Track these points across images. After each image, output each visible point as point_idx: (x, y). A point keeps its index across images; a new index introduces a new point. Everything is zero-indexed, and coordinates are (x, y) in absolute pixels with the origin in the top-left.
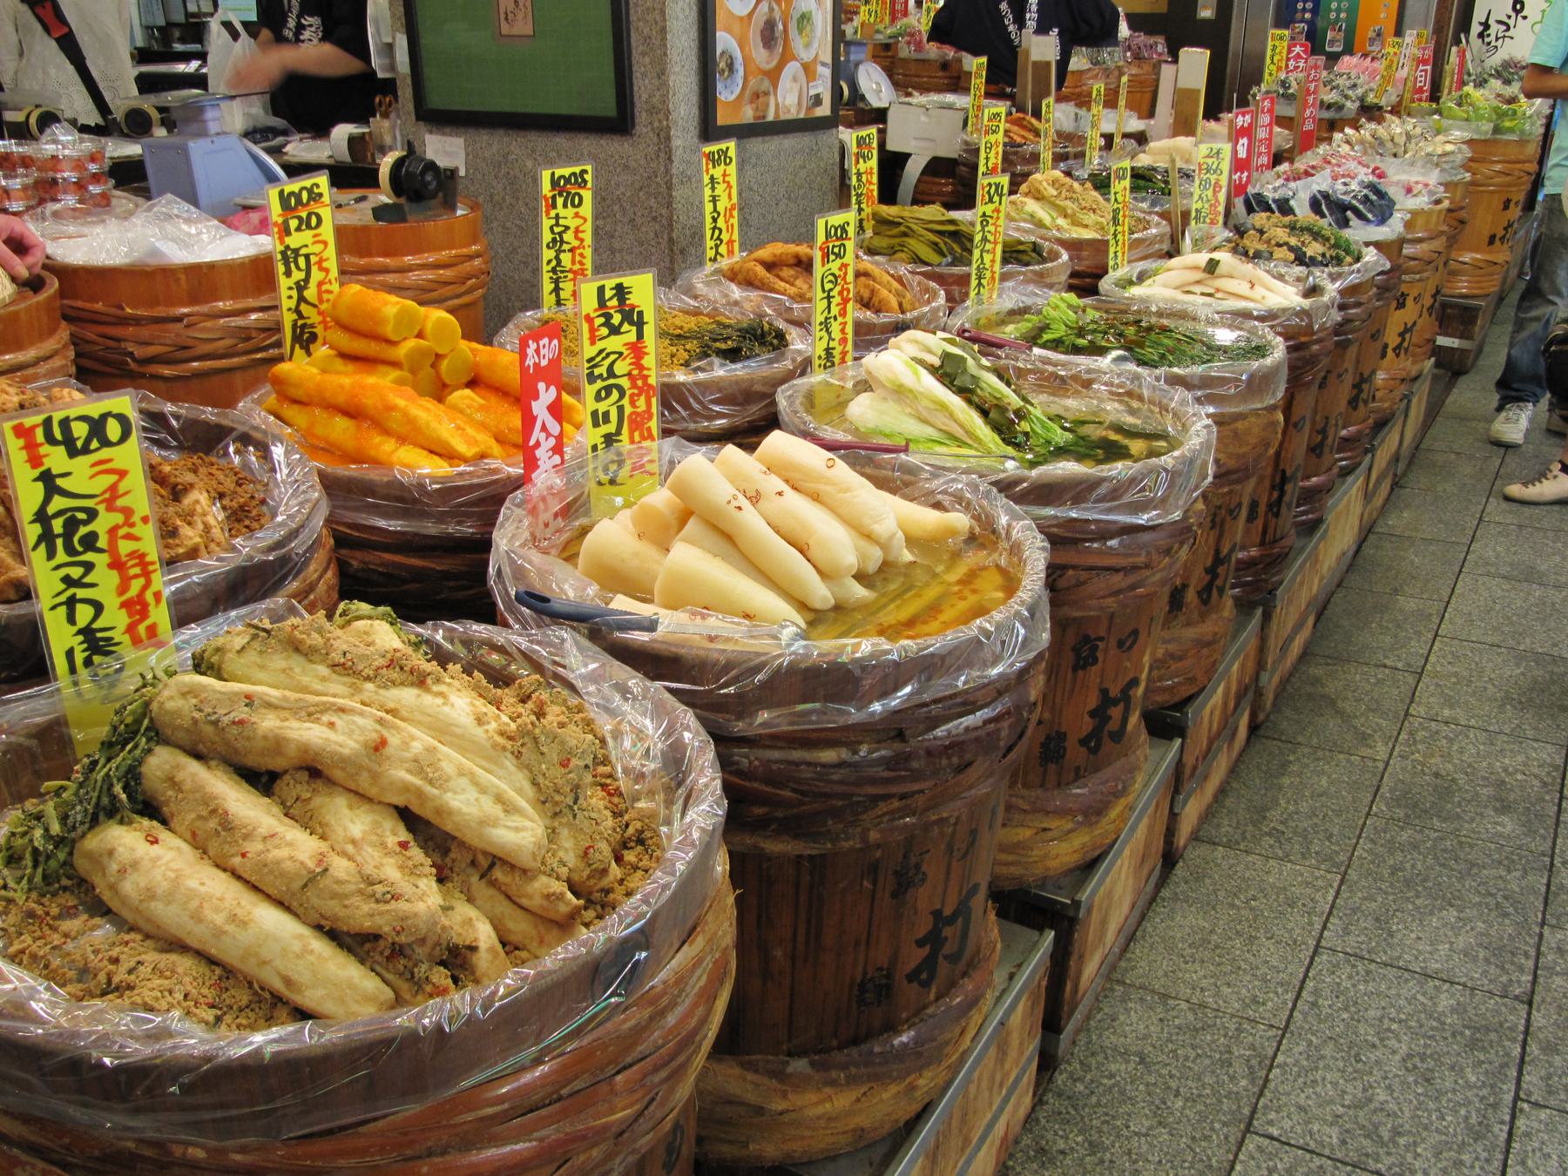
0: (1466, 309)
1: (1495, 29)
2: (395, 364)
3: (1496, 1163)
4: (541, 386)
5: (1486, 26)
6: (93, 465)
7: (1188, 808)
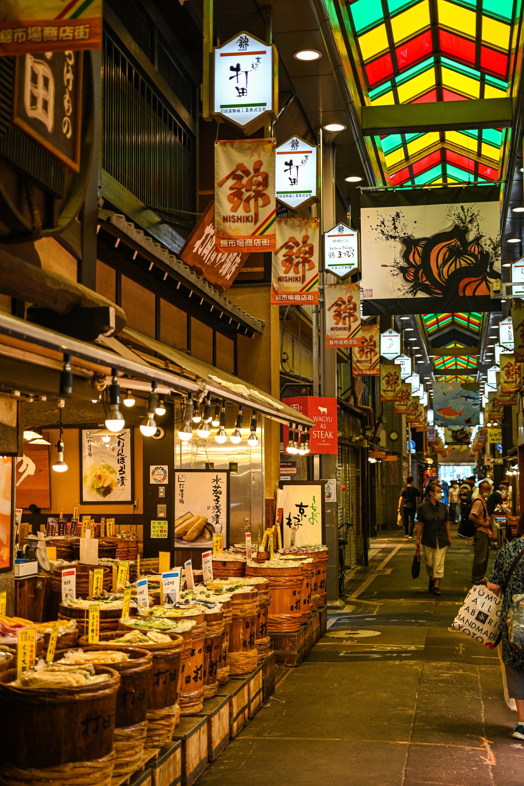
1: (293, 521)
5: (289, 519)
6: (358, 634)
7: (381, 435)
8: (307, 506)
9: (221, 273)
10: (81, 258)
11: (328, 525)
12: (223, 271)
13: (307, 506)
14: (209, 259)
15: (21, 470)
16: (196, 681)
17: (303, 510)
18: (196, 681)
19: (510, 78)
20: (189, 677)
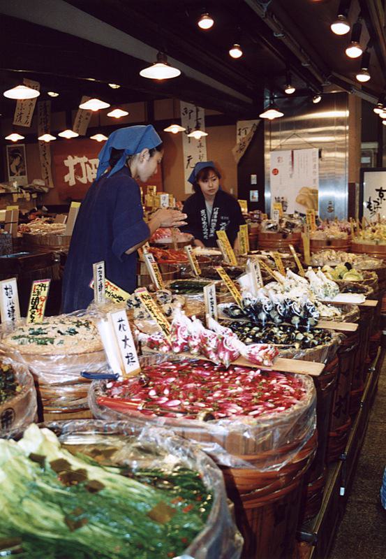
5: (370, 203)
11: (242, 495)
19: (357, 215)
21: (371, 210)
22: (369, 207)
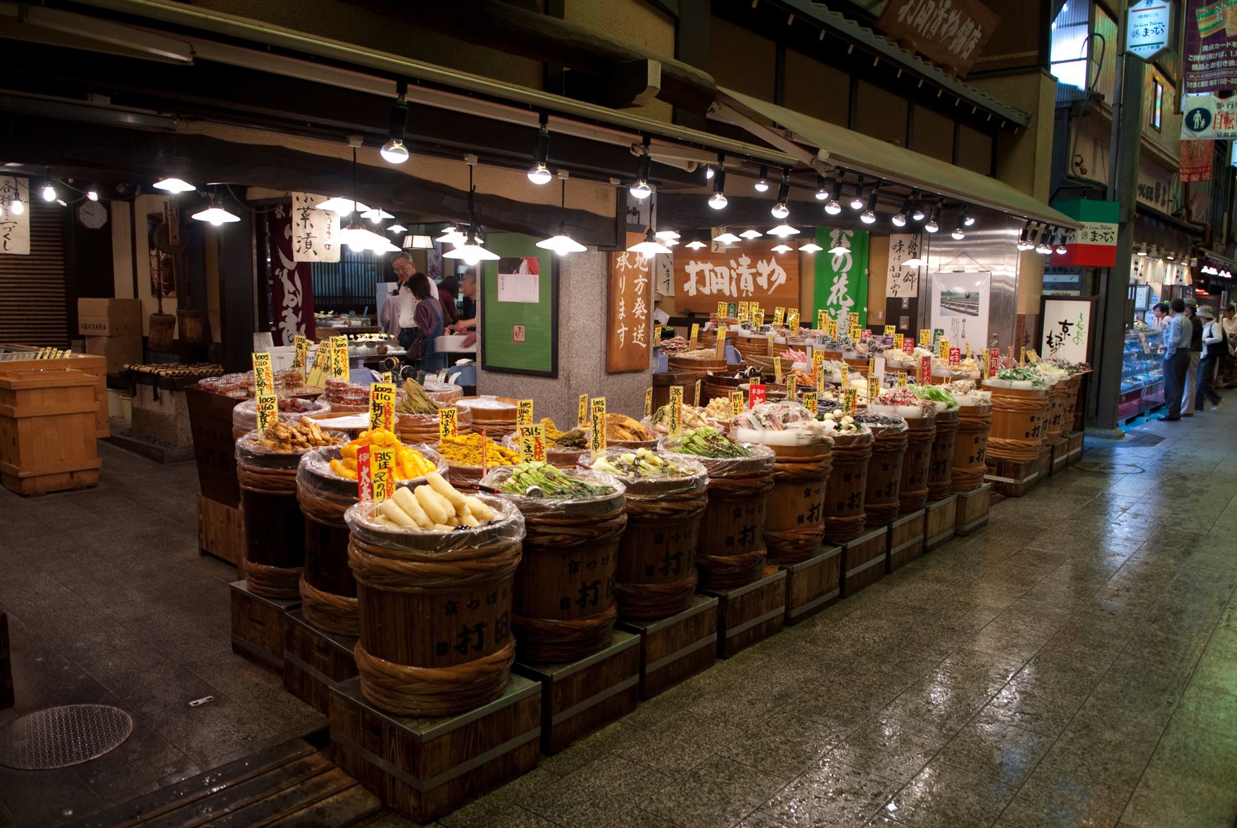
0: (1015, 465)
1: (1054, 340)
2: (833, 449)
3: (1011, 806)
4: (364, 467)
5: (1050, 338)
8: (1072, 324)
9: (952, 50)
10: (678, 15)
12: (956, 46)
13: (1072, 324)
14: (928, 32)
15: (773, 279)
16: (811, 521)
17: (1067, 328)
18: (811, 521)
20: (802, 516)
21: (1052, 347)
22: (1049, 342)
